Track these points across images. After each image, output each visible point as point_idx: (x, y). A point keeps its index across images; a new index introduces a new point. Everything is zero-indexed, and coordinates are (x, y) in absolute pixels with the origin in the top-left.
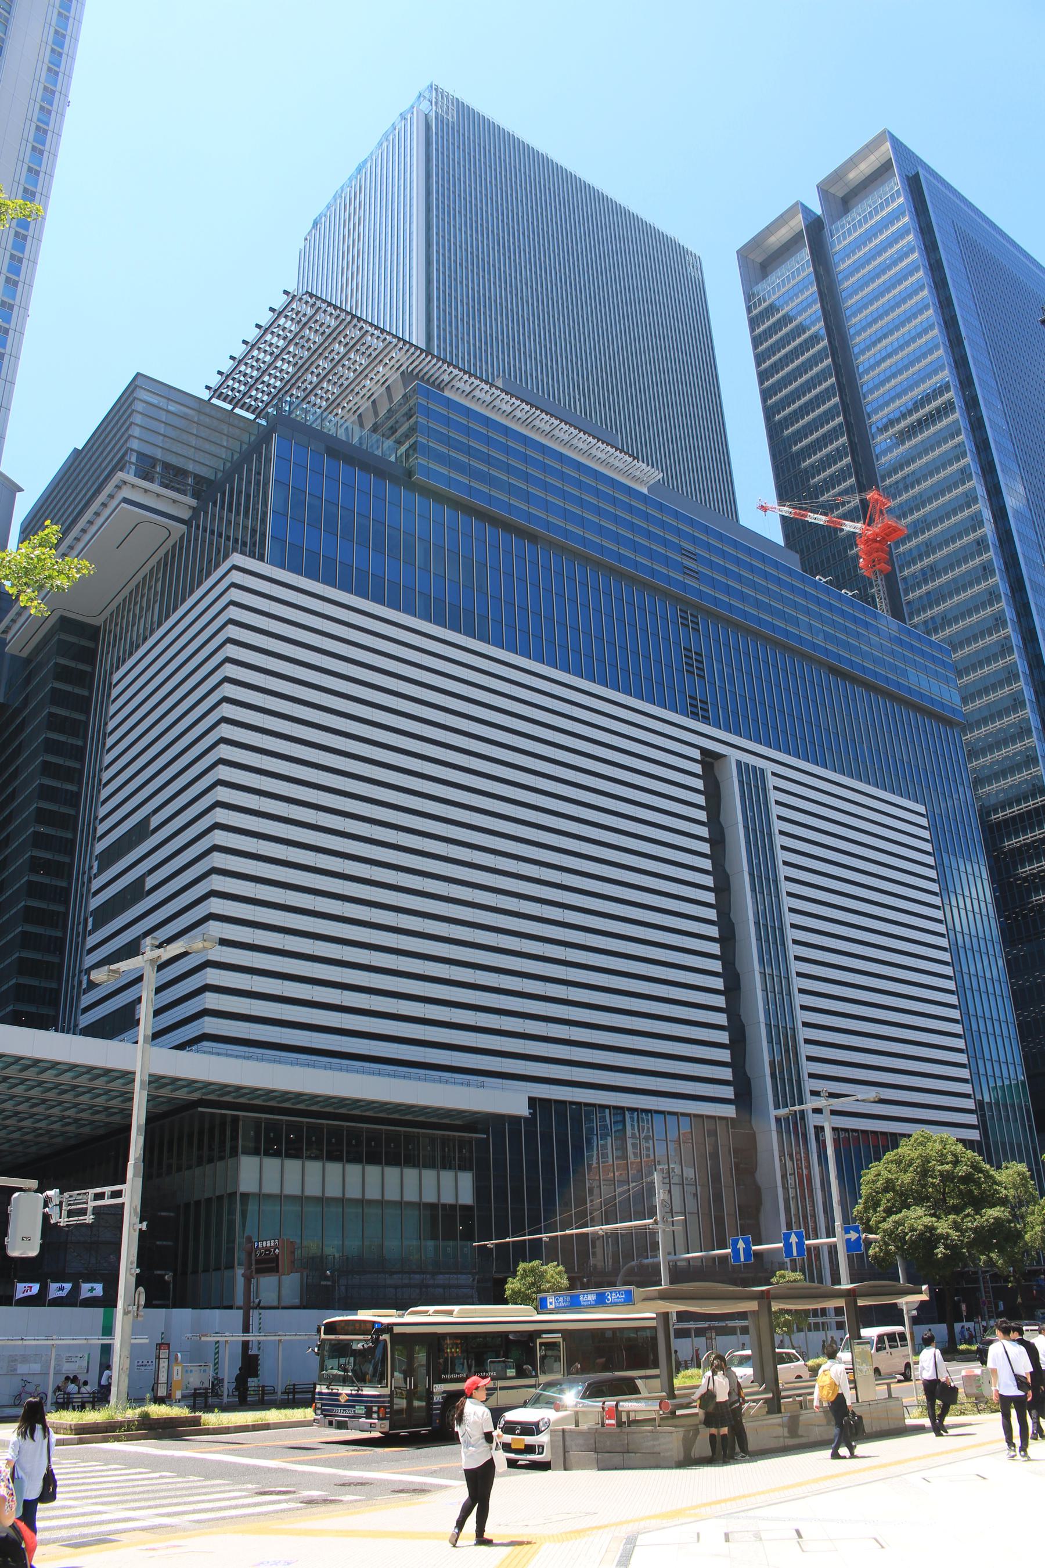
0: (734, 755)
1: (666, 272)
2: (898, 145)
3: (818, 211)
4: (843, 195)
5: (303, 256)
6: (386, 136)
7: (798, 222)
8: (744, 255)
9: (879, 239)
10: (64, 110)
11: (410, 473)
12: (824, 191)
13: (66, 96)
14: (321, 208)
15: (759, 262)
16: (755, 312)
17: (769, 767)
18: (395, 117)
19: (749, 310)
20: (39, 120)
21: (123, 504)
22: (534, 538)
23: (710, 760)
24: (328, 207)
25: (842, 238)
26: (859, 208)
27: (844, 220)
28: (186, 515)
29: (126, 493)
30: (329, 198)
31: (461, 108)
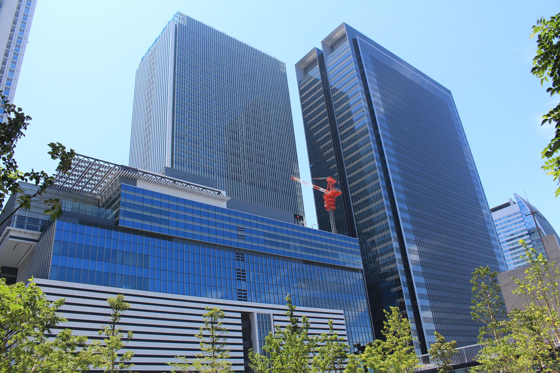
0: (256, 311)
1: (275, 68)
2: (348, 28)
3: (321, 49)
4: (332, 43)
5: (138, 72)
6: (164, 30)
7: (315, 55)
8: (298, 65)
9: (341, 64)
10: (26, 45)
11: (117, 222)
12: (324, 43)
13: (27, 39)
14: (144, 54)
15: (304, 67)
16: (301, 88)
17: (271, 312)
18: (166, 23)
19: (299, 87)
20: (15, 50)
21: (10, 239)
22: (170, 238)
23: (246, 317)
24: (146, 54)
25: (331, 61)
26: (339, 48)
27: (332, 54)
28: (37, 238)
29: (11, 234)
30: (146, 51)
31: (190, 20)
